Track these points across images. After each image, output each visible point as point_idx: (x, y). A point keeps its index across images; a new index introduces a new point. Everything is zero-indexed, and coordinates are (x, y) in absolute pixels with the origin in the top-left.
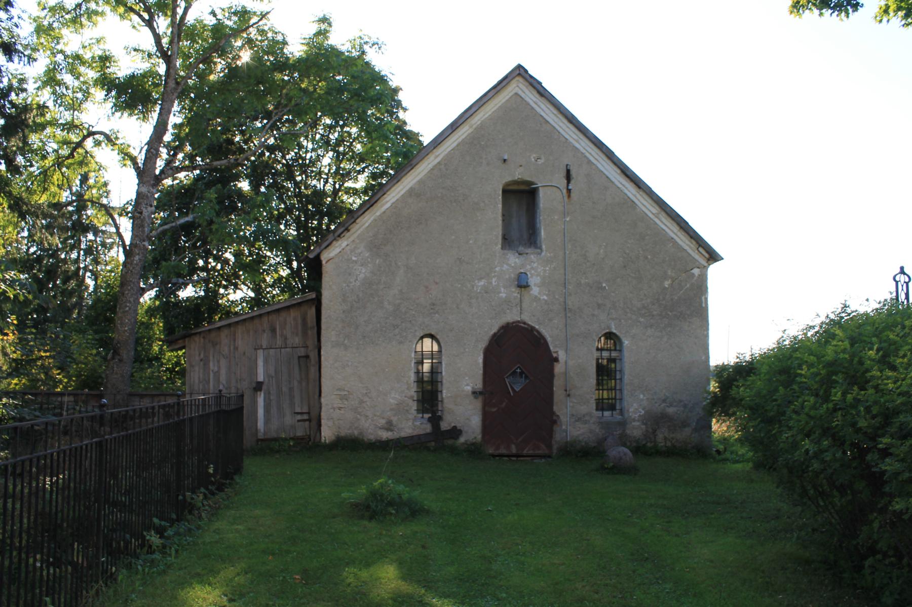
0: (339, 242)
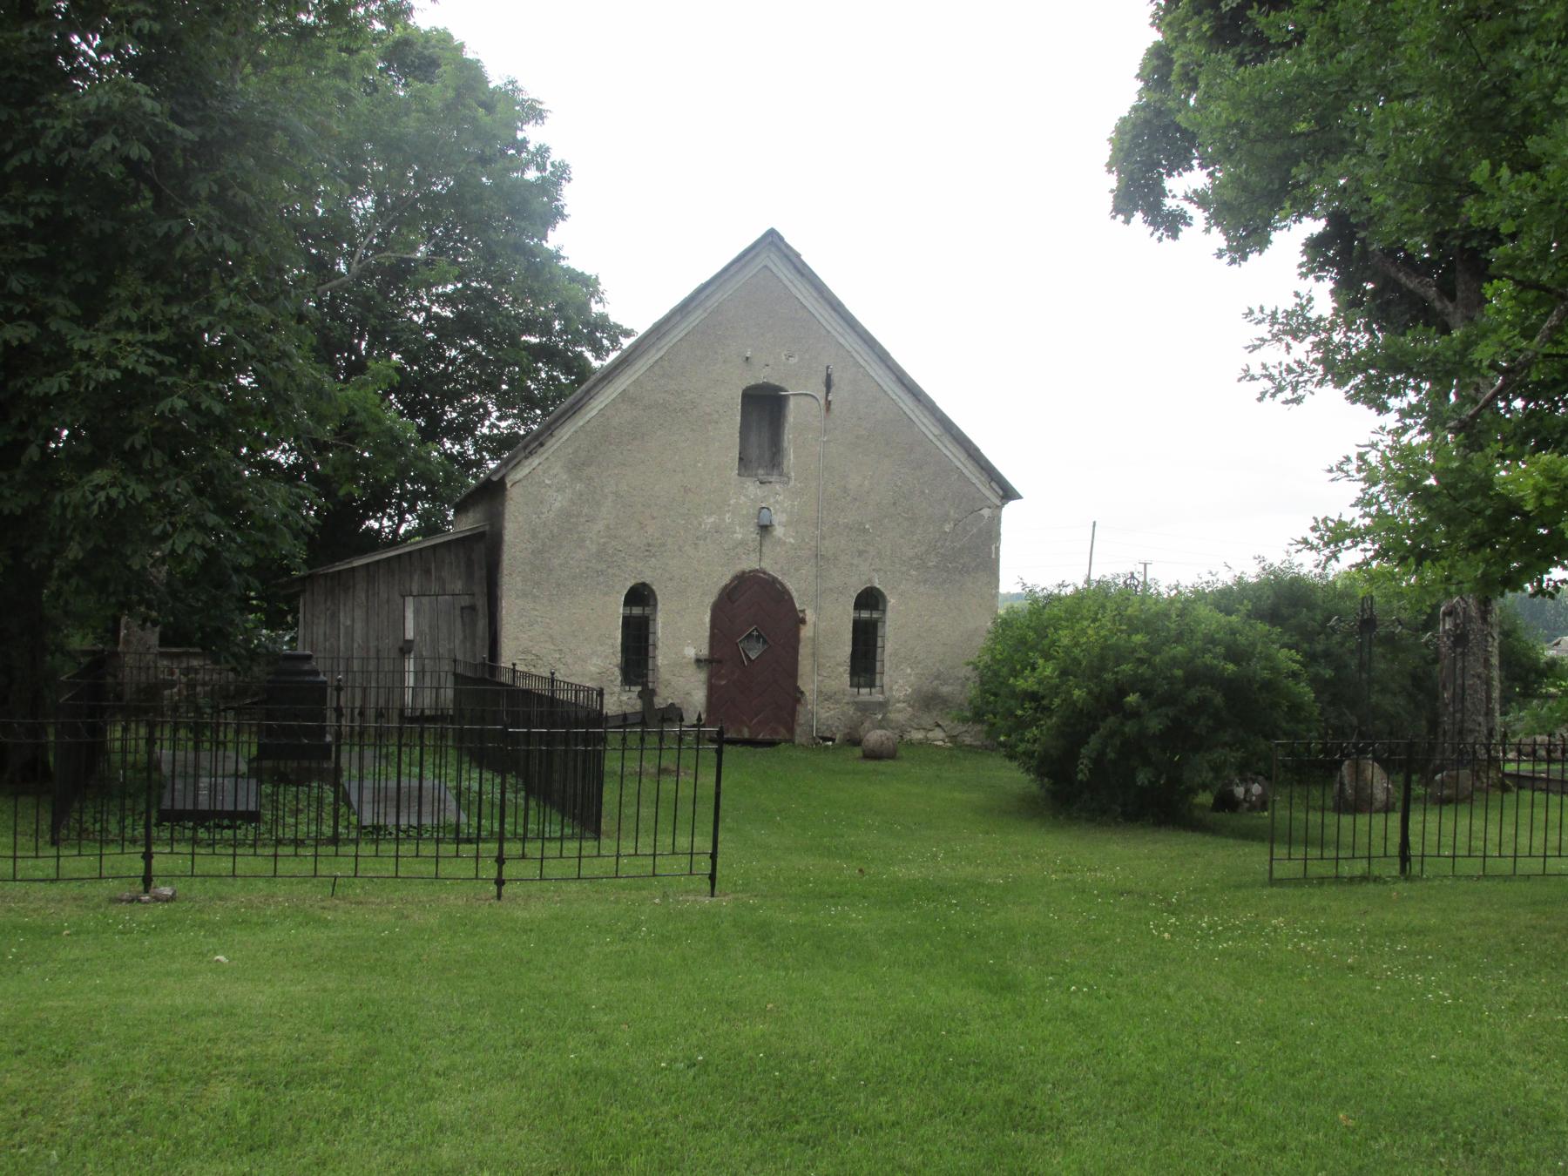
0: (530, 460)
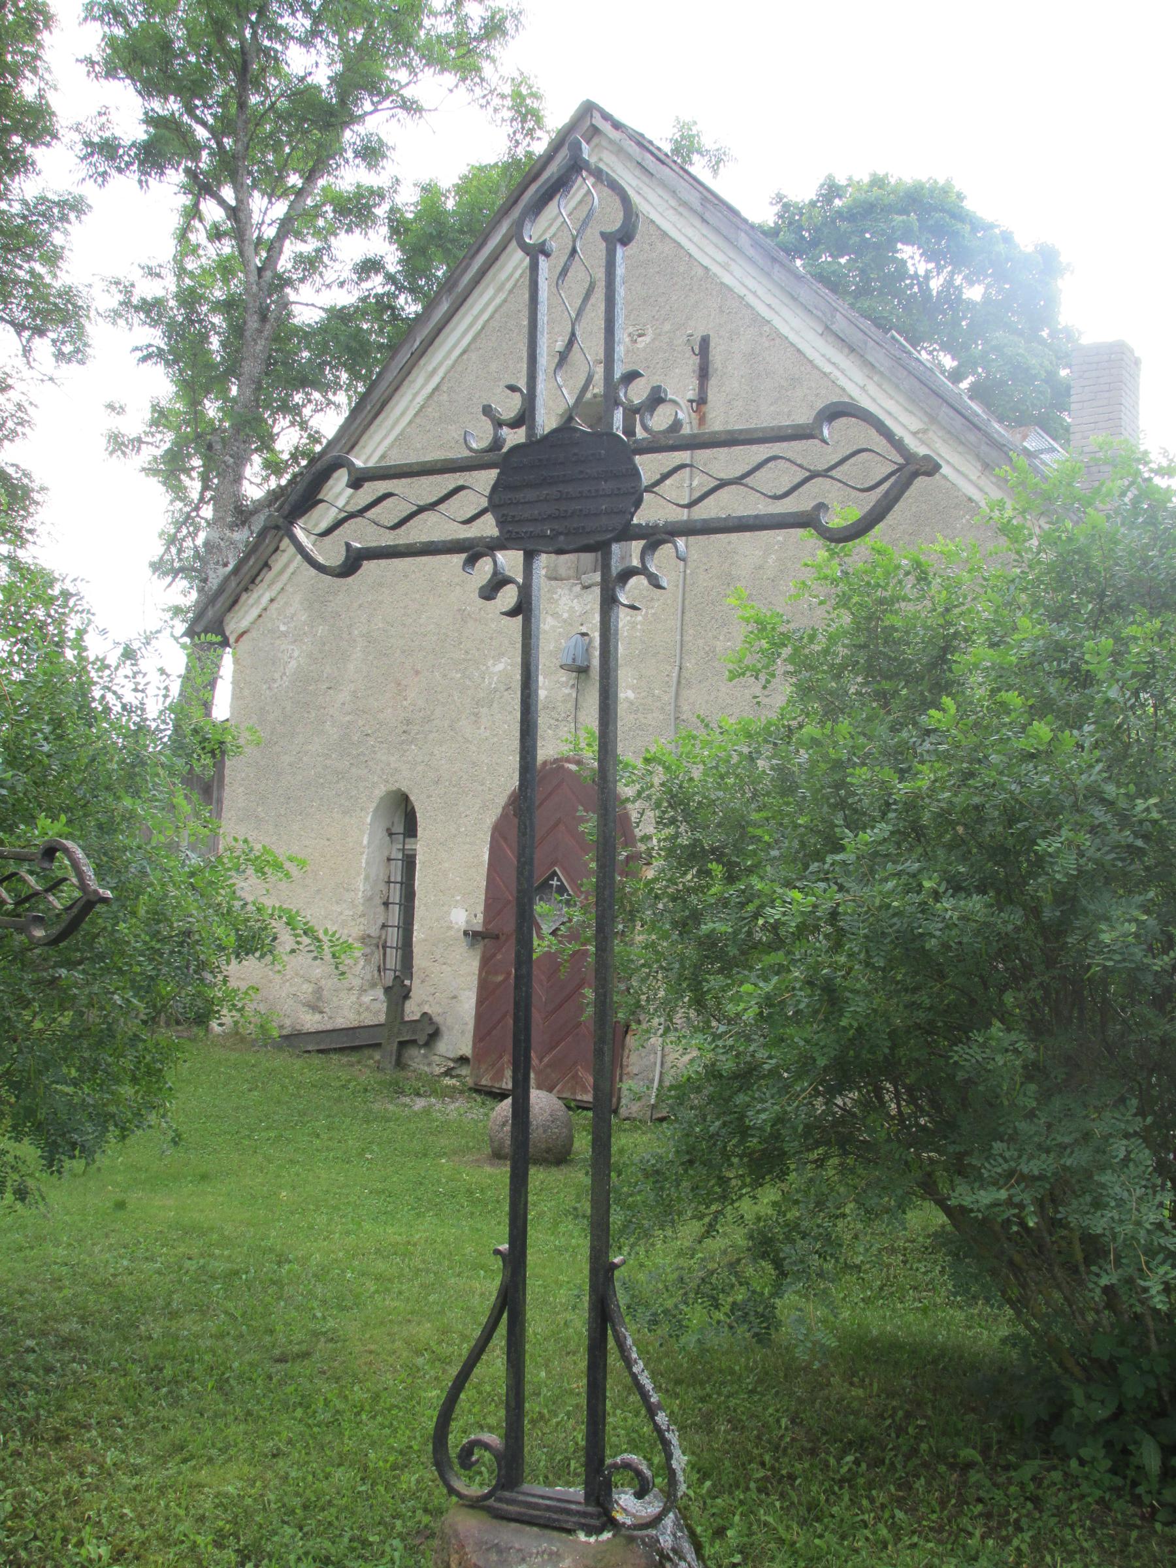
0: (255, 595)
